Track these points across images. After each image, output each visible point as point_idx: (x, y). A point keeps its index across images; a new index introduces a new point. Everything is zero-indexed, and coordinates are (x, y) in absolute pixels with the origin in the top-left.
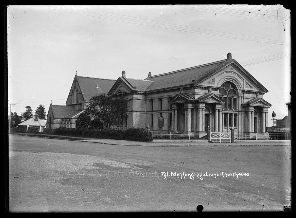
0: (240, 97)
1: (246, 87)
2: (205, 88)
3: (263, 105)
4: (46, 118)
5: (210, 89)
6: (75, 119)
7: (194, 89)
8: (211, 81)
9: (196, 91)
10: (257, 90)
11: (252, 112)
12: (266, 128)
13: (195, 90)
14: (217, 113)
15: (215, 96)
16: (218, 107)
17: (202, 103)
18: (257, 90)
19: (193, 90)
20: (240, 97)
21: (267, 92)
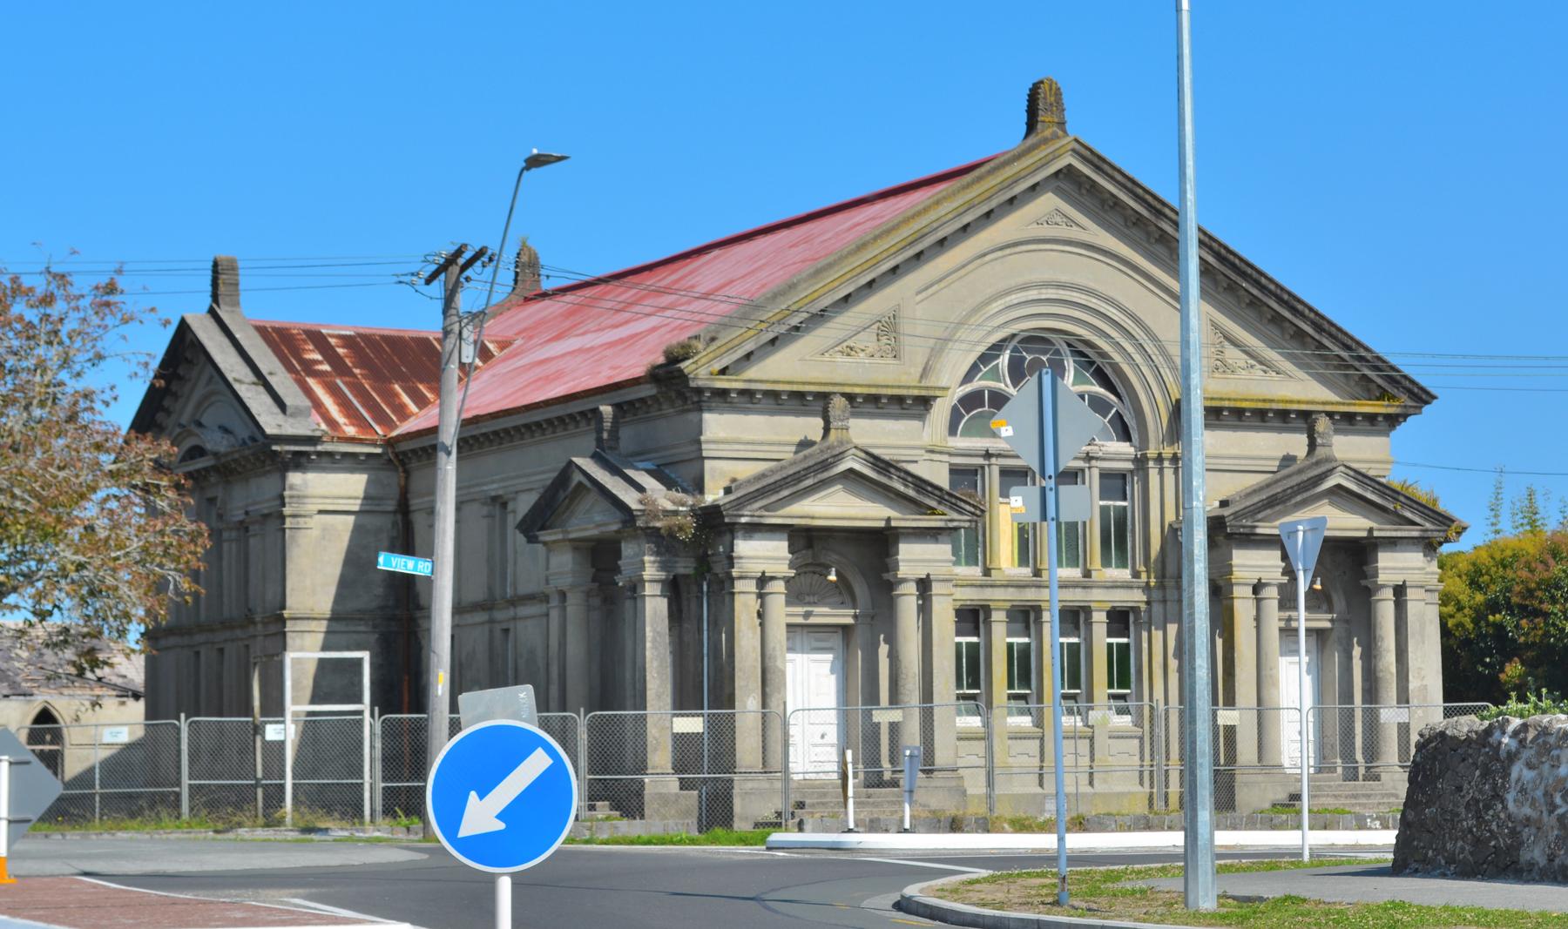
0: (1159, 459)
1: (1222, 367)
2: (799, 396)
3: (888, 512)
4: (1467, 724)
5: (1323, 424)
6: (1220, 713)
7: (701, 410)
8: (867, 340)
9: (717, 426)
10: (1335, 398)
11: (1257, 588)
12: (872, 709)
13: (708, 417)
14: (908, 603)
15: (1360, 477)
16: (913, 559)
17: (755, 529)
18: (1335, 398)
19: (692, 416)
20: (1159, 459)
21: (1426, 409)
